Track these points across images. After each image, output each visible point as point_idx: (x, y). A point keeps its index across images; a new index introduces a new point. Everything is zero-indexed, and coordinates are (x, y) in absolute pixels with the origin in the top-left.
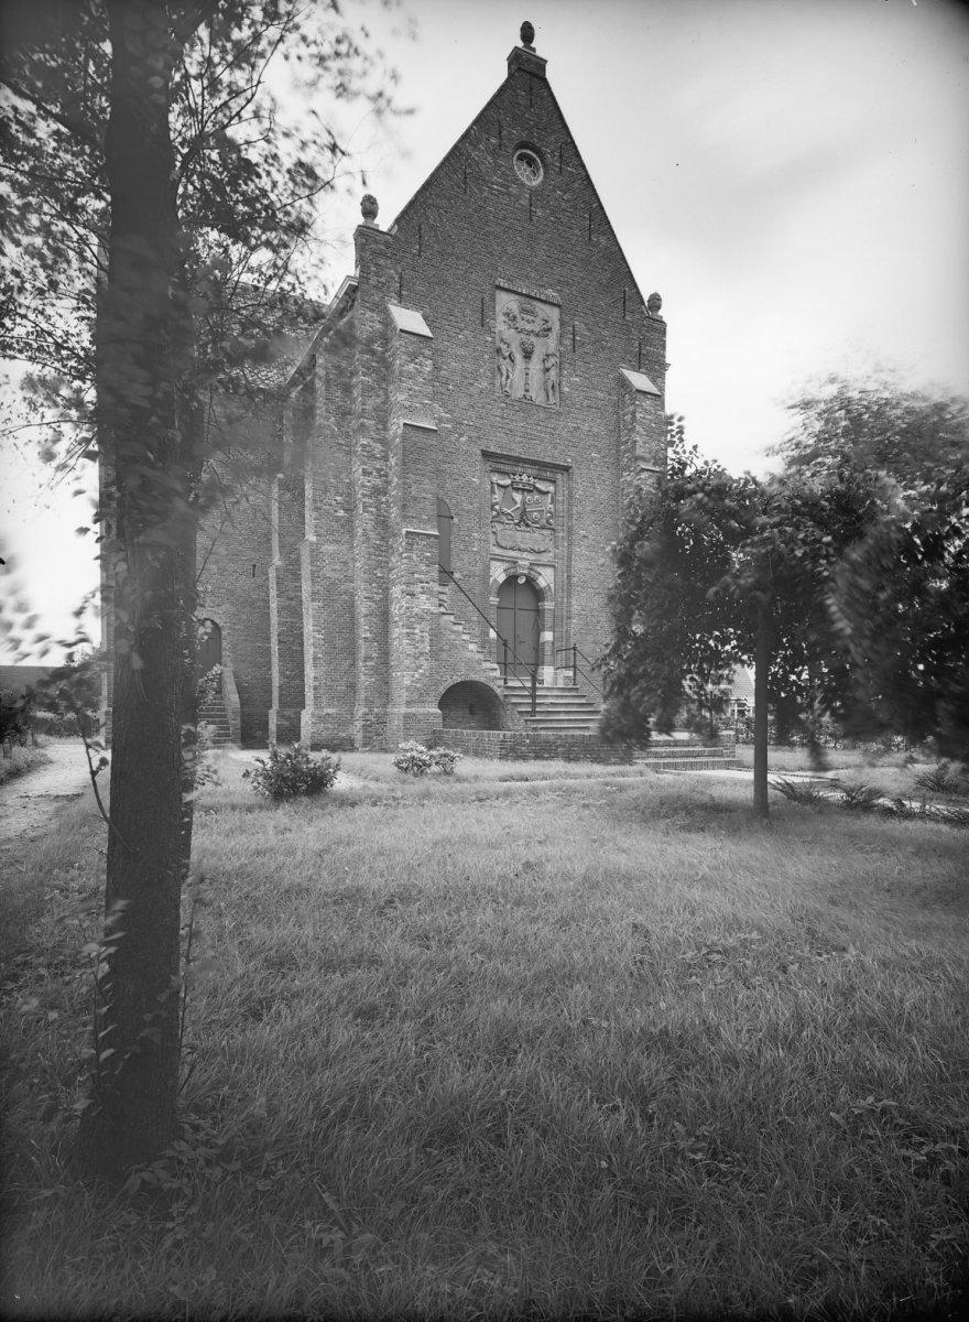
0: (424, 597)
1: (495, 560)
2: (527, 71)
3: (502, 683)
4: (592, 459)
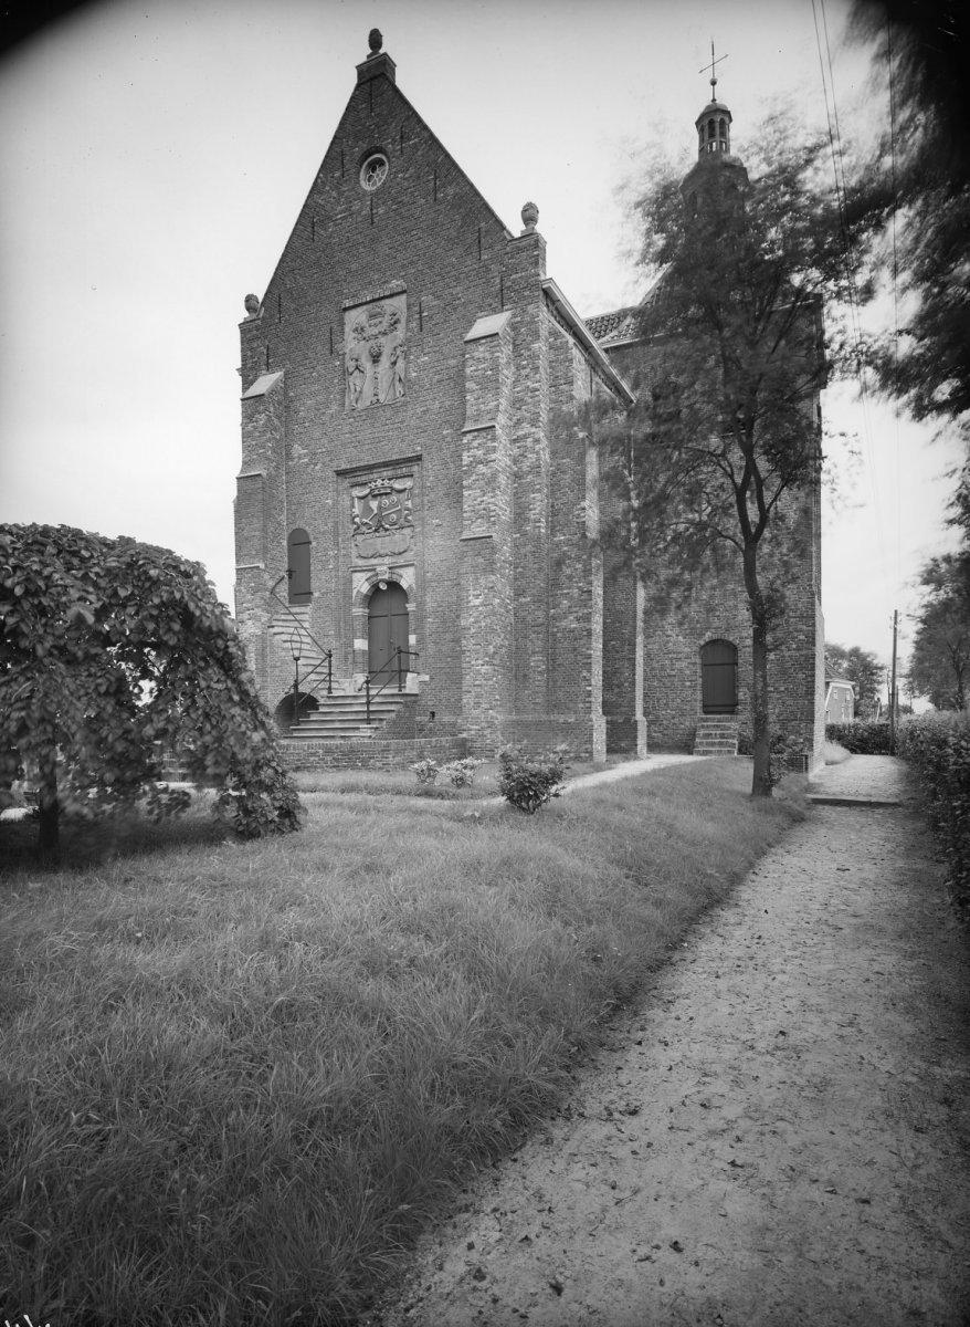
0: (250, 622)
1: (355, 571)
2: (376, 77)
3: (325, 693)
4: (444, 437)
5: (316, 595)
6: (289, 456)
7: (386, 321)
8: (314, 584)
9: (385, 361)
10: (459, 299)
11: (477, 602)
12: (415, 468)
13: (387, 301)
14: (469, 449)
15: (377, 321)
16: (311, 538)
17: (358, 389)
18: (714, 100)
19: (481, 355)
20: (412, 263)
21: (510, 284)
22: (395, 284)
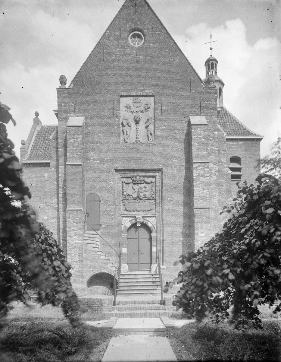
0: (75, 237)
1: (124, 217)
5: (103, 226)
6: (88, 158)
7: (142, 108)
8: (102, 220)
9: (142, 125)
10: (181, 106)
11: (203, 235)
12: (157, 174)
13: (144, 98)
14: (196, 171)
15: (138, 105)
16: (101, 199)
17: (128, 133)
18: (211, 56)
19: (199, 132)
20: (157, 85)
21: (204, 105)
22: (148, 91)
